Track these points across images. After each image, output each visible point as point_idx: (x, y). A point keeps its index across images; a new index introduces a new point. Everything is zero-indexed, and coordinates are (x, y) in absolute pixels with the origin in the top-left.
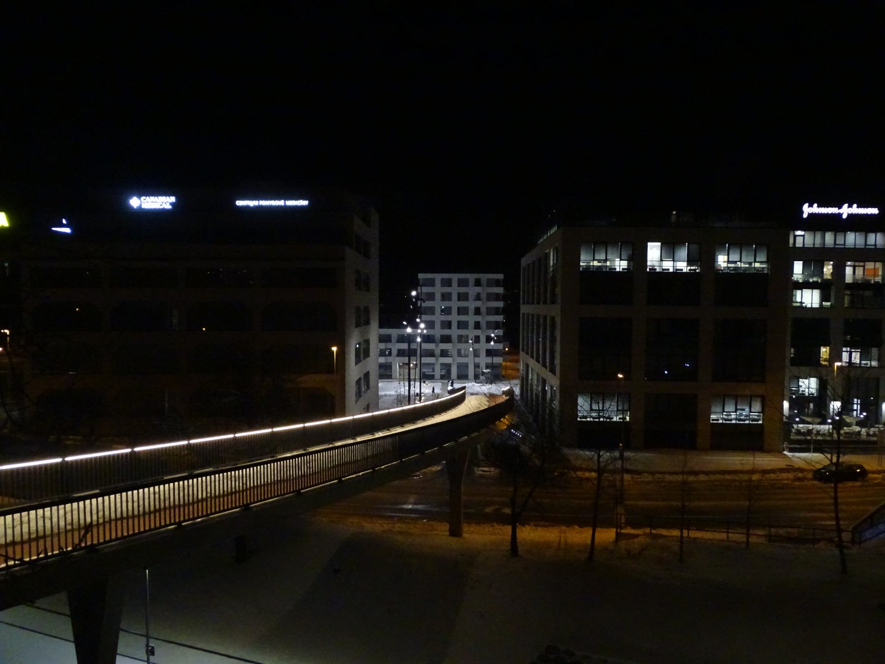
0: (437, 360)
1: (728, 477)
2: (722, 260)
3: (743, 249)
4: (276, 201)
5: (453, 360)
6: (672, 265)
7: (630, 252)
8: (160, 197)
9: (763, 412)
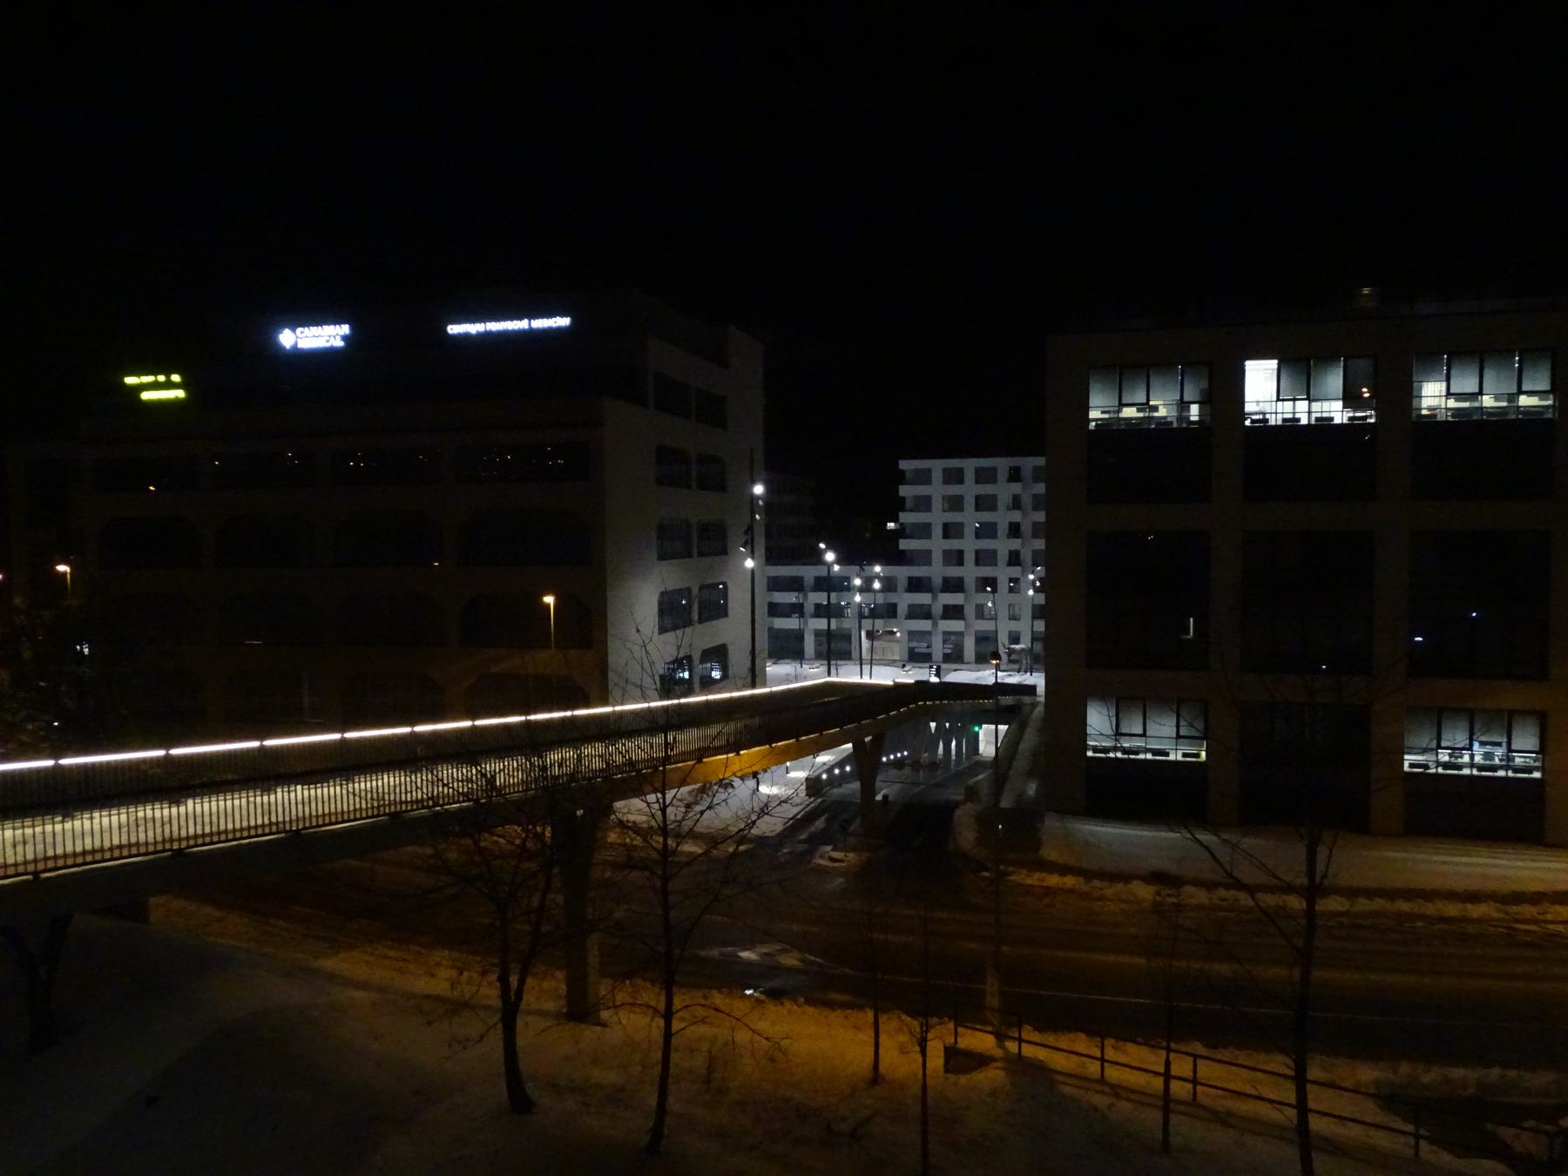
0: (935, 625)
1: (1404, 906)
2: (1432, 395)
3: (1486, 365)
4: (515, 322)
5: (967, 626)
6: (1291, 403)
7: (1204, 384)
8: (325, 327)
9: (1542, 750)
